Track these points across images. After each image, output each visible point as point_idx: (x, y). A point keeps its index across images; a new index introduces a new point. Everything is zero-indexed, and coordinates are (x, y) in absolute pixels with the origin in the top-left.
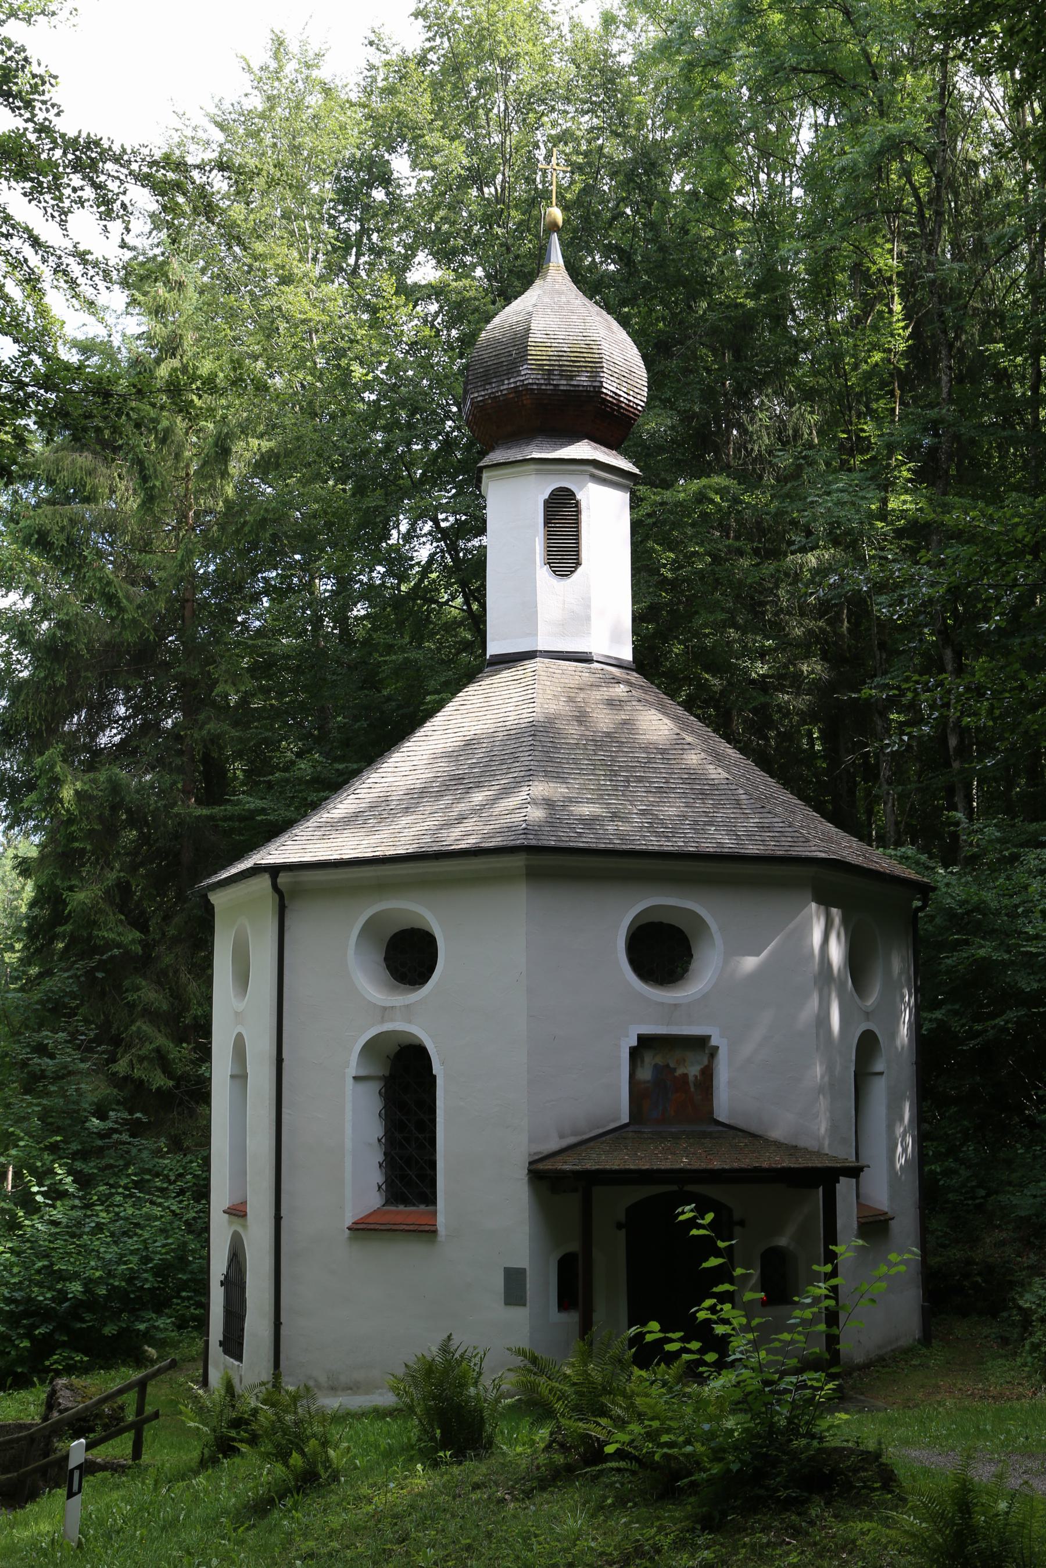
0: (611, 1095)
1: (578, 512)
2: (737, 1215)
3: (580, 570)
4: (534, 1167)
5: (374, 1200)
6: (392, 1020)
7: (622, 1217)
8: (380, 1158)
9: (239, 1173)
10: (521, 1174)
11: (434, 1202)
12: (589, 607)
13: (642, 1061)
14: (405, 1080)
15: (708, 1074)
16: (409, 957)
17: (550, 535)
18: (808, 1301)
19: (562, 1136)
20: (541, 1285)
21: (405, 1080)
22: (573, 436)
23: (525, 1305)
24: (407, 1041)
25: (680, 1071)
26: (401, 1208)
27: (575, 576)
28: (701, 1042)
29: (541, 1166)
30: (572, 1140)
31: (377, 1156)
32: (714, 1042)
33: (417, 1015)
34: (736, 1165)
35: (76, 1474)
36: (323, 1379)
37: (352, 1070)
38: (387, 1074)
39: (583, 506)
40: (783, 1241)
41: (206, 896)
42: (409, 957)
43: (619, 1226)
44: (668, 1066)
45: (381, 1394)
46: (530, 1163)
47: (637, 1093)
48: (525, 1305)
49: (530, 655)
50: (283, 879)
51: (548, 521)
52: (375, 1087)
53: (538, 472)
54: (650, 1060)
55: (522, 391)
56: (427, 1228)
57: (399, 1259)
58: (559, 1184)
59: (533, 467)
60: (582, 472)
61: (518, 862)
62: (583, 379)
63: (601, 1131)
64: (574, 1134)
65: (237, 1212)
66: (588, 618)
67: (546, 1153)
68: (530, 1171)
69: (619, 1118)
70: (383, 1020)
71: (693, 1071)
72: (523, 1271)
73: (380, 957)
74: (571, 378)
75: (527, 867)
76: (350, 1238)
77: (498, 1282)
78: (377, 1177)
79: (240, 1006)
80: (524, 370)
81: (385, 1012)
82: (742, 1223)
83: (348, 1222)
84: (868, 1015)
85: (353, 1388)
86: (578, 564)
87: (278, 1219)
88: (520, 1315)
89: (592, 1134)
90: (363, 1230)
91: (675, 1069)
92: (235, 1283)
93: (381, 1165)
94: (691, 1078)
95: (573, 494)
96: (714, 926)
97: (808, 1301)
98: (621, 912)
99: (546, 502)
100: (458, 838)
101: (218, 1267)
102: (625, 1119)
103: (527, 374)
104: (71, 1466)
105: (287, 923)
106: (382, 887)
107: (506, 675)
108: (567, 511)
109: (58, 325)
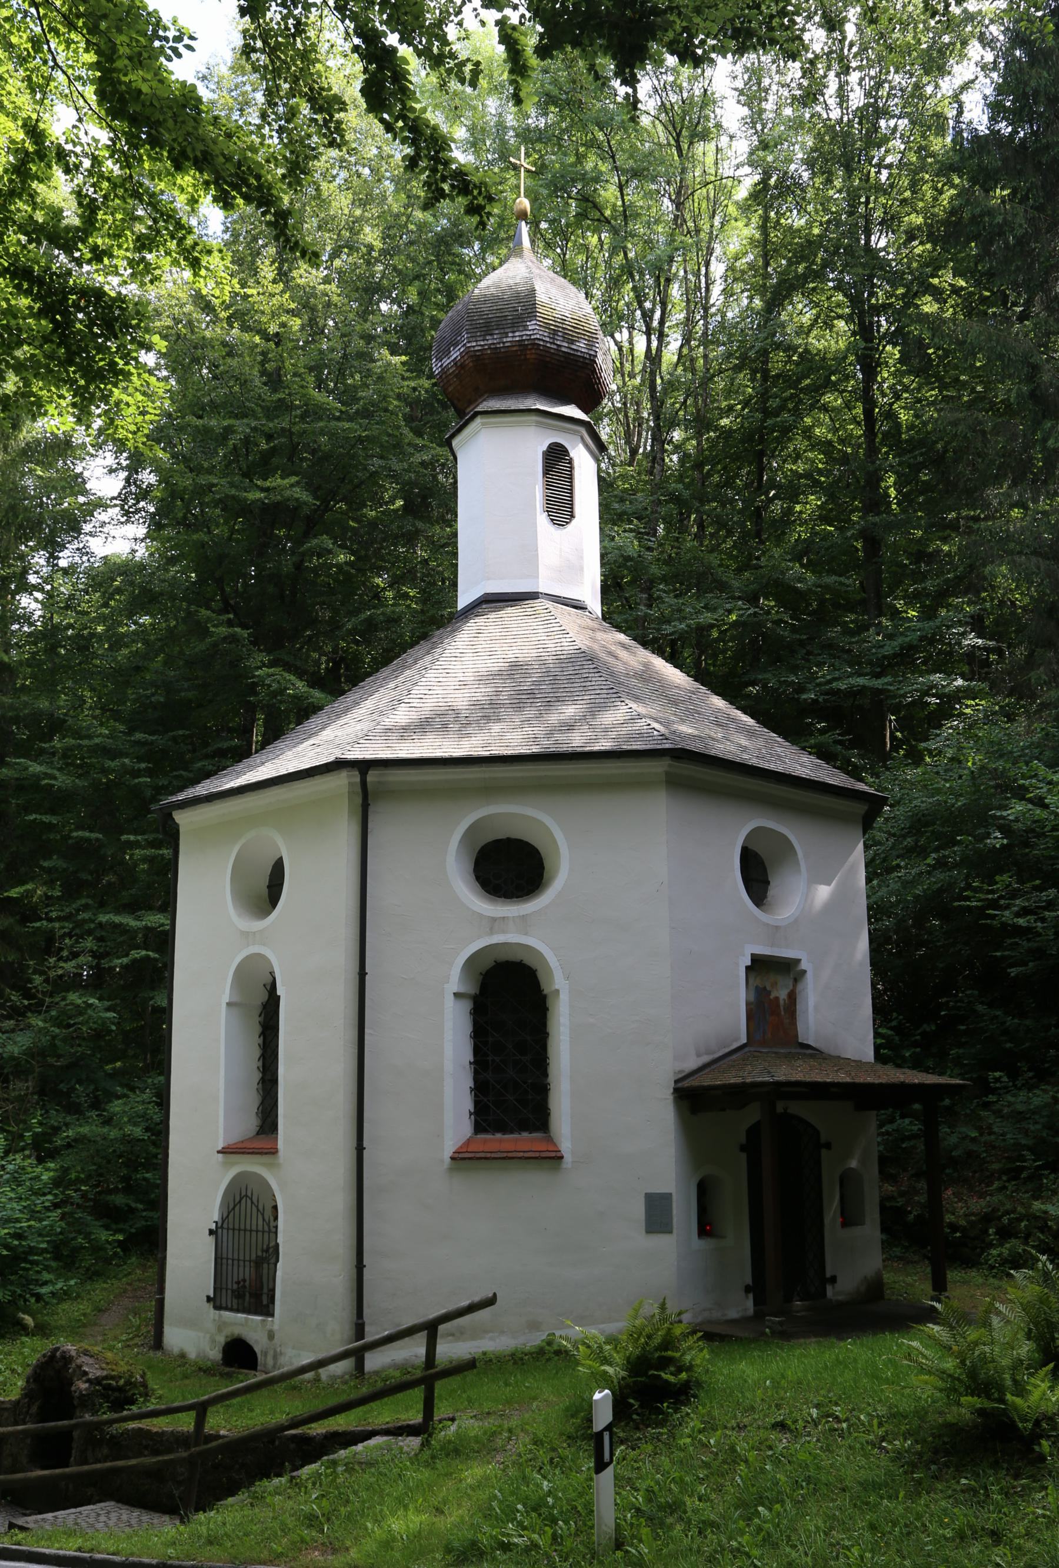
0: (727, 1013)
1: (572, 468)
2: (823, 1139)
3: (574, 522)
4: (680, 1085)
5: (466, 1128)
6: (504, 932)
7: (743, 1139)
10: (666, 1094)
12: (582, 558)
16: (510, 868)
17: (548, 485)
19: (698, 1055)
20: (683, 1213)
22: (566, 401)
23: (671, 1232)
27: (570, 527)
29: (685, 1084)
30: (706, 1059)
32: (804, 966)
34: (869, 1080)
39: (576, 464)
40: (854, 1164)
41: (170, 816)
42: (510, 868)
44: (765, 988)
45: (492, 1339)
46: (676, 1082)
48: (671, 1232)
49: (533, 596)
50: (372, 776)
51: (546, 472)
52: (466, 1006)
53: (539, 424)
55: (523, 346)
56: (553, 1154)
57: (514, 1193)
59: (534, 418)
60: (575, 433)
61: (659, 767)
62: (581, 345)
63: (727, 1050)
66: (581, 569)
67: (687, 1071)
68: (676, 1090)
69: (737, 1039)
70: (492, 932)
72: (667, 1197)
73: (471, 867)
74: (572, 342)
75: (667, 774)
76: (451, 1170)
77: (638, 1210)
80: (531, 325)
82: (828, 1146)
86: (572, 516)
87: (360, 1149)
89: (720, 1054)
90: (462, 1159)
94: (782, 1002)
95: (567, 451)
96: (800, 854)
98: (730, 831)
100: (577, 741)
103: (533, 330)
105: (370, 826)
106: (489, 791)
107: (510, 611)
108: (563, 466)
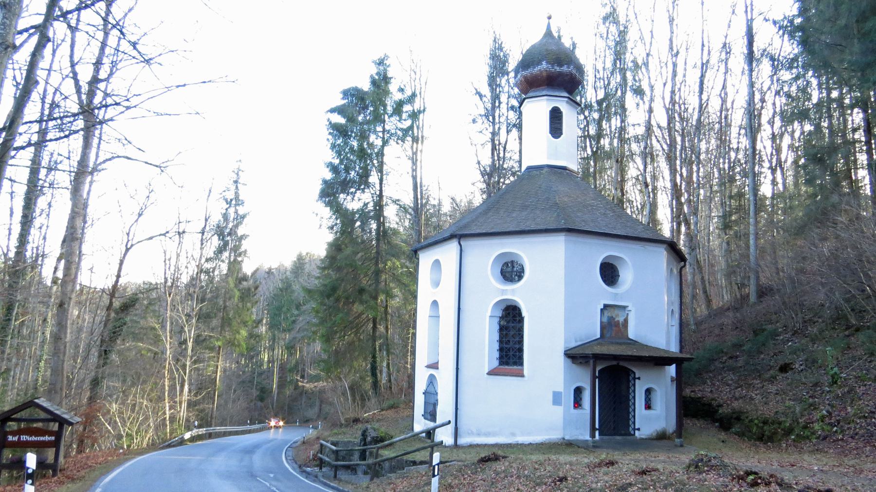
5: (496, 363)
9: (434, 345)
11: (522, 364)
14: (511, 320)
15: (626, 321)
18: (619, 93)
21: (511, 320)
28: (624, 307)
30: (579, 343)
31: (496, 346)
32: (629, 309)
33: (515, 293)
36: (474, 431)
37: (489, 314)
47: (603, 328)
54: (607, 313)
71: (621, 319)
72: (560, 393)
77: (550, 397)
78: (497, 355)
81: (503, 292)
83: (487, 371)
85: (487, 434)
88: (559, 410)
97: (619, 93)
101: (420, 386)
102: (599, 336)
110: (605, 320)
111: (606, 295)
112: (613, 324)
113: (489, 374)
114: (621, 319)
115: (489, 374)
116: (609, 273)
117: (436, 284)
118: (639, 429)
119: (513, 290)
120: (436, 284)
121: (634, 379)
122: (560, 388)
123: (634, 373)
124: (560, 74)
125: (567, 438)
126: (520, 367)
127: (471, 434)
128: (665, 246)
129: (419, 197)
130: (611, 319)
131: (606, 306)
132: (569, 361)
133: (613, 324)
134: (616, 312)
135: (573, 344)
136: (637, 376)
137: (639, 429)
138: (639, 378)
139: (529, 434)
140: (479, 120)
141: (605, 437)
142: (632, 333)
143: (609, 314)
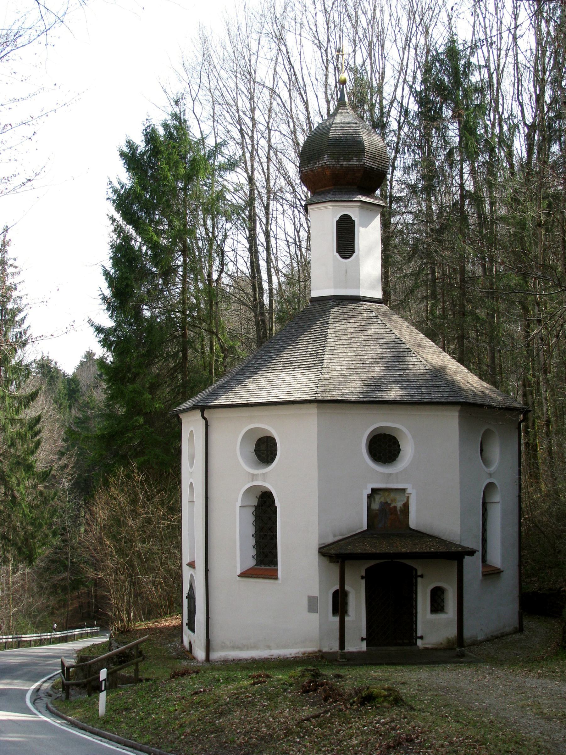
3: (354, 255)
6: (257, 480)
7: (363, 574)
8: (254, 543)
11: (276, 564)
13: (375, 500)
14: (264, 509)
15: (406, 506)
19: (334, 536)
21: (264, 509)
24: (264, 490)
25: (392, 505)
26: (263, 567)
28: (404, 490)
30: (340, 538)
32: (408, 491)
33: (270, 478)
35: (103, 683)
36: (228, 643)
37: (239, 504)
38: (256, 504)
43: (362, 578)
58: (337, 554)
64: (341, 535)
65: (192, 565)
70: (253, 481)
71: (399, 505)
77: (305, 602)
79: (191, 470)
81: (254, 477)
83: (239, 573)
84: (490, 475)
88: (315, 617)
91: (390, 504)
92: (191, 597)
93: (254, 547)
94: (398, 508)
99: (337, 222)
102: (365, 528)
104: (101, 679)
109: (53, 363)
110: (376, 506)
111: (378, 475)
112: (387, 512)
113: (243, 575)
114: (399, 505)
115: (243, 575)
116: (384, 448)
117: (191, 465)
118: (421, 638)
119: (264, 475)
120: (191, 465)
121: (417, 576)
122: (315, 592)
123: (416, 570)
124: (349, 169)
125: (325, 650)
126: (273, 567)
127: (224, 647)
128: (458, 408)
129: (263, 264)
130: (385, 506)
131: (375, 491)
132: (325, 560)
133: (387, 512)
134: (392, 495)
135: (331, 540)
136: (419, 573)
137: (421, 638)
138: (422, 576)
139: (286, 647)
140: (462, 17)
141: (373, 648)
142: (415, 520)
143: (382, 500)
